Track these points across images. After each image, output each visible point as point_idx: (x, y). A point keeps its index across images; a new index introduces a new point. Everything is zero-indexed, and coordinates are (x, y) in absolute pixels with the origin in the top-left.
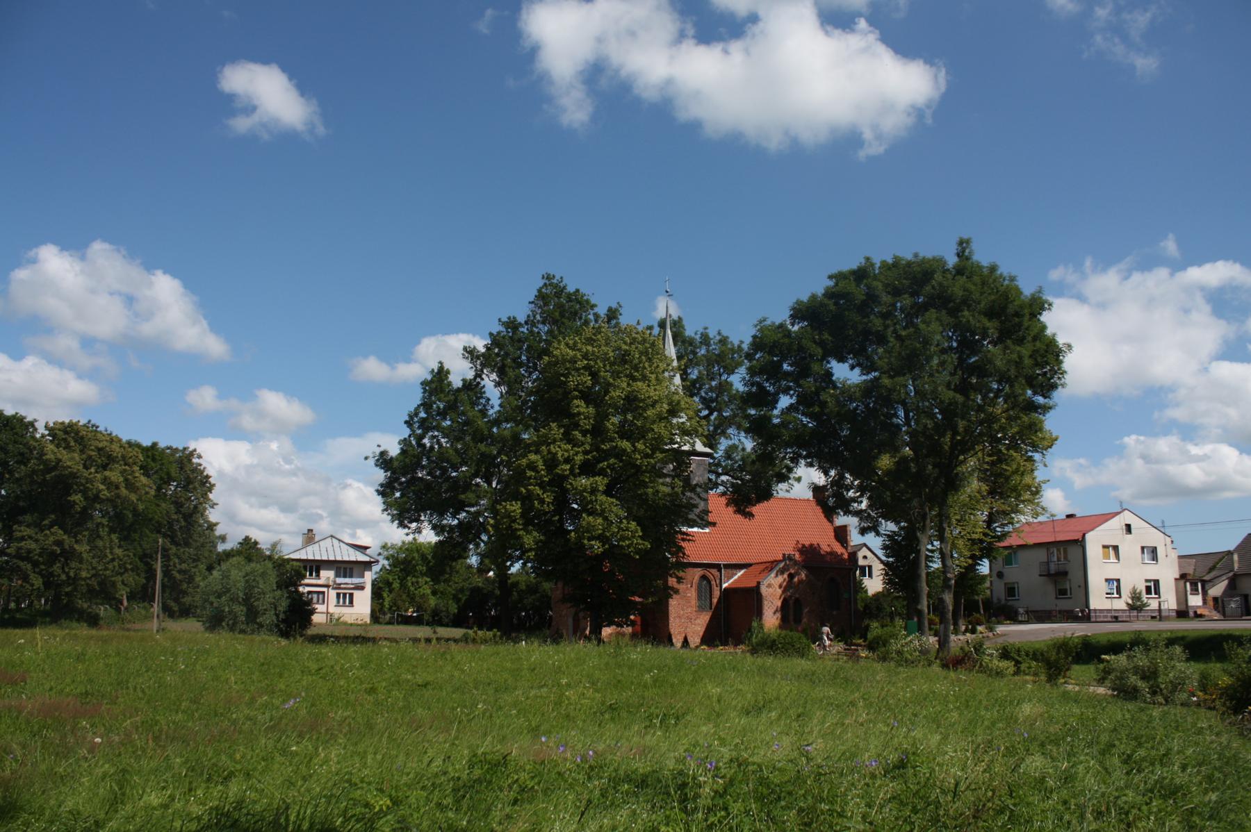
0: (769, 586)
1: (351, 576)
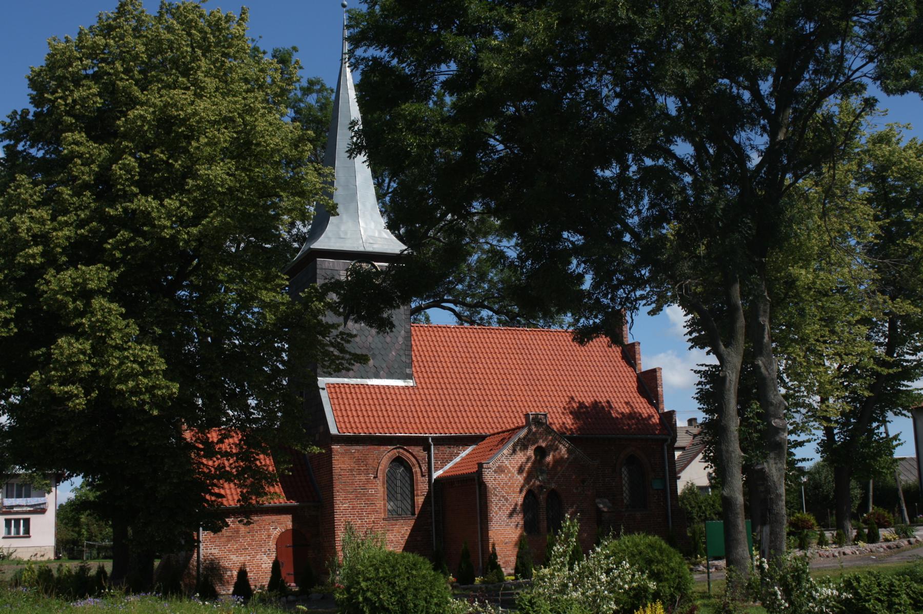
0: (500, 470)
1: (28, 495)
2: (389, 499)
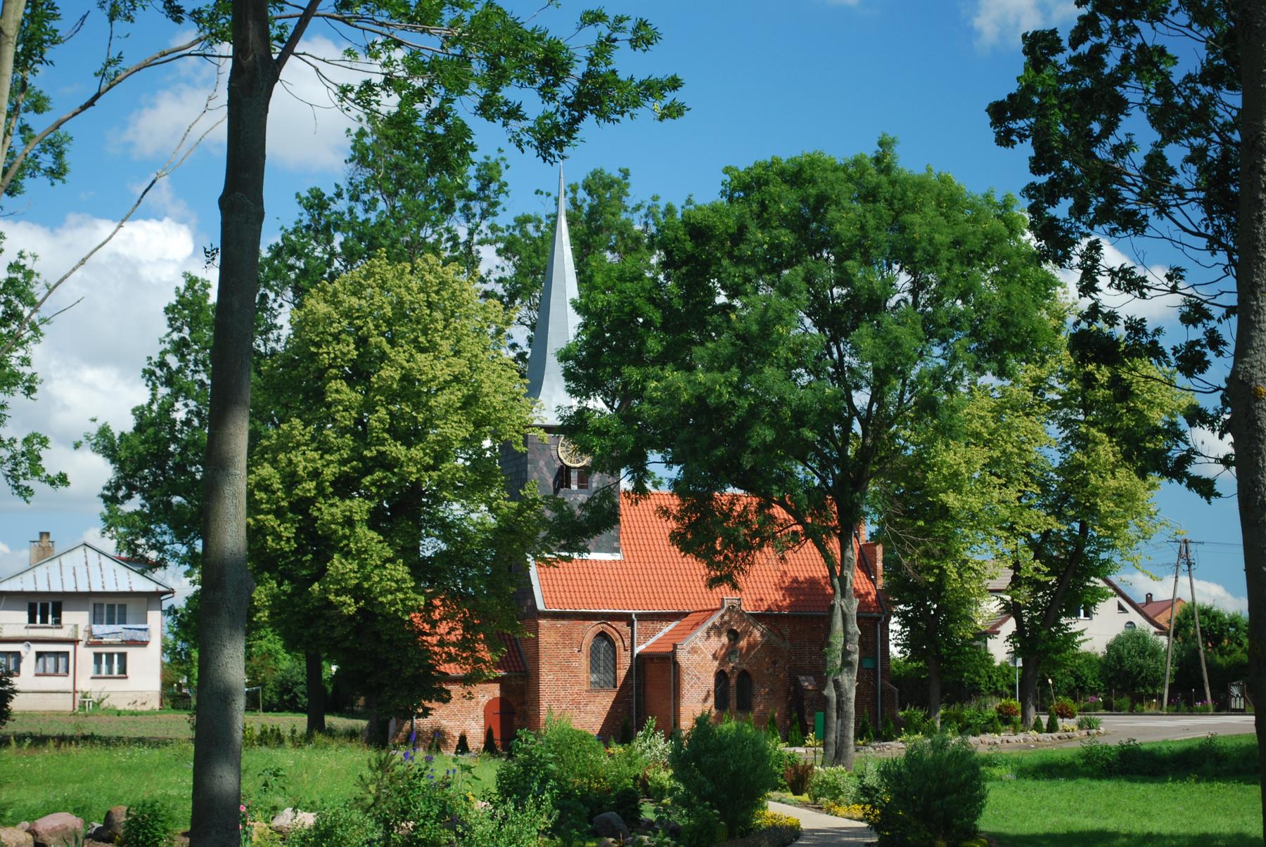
0: (694, 651)
2: (592, 672)
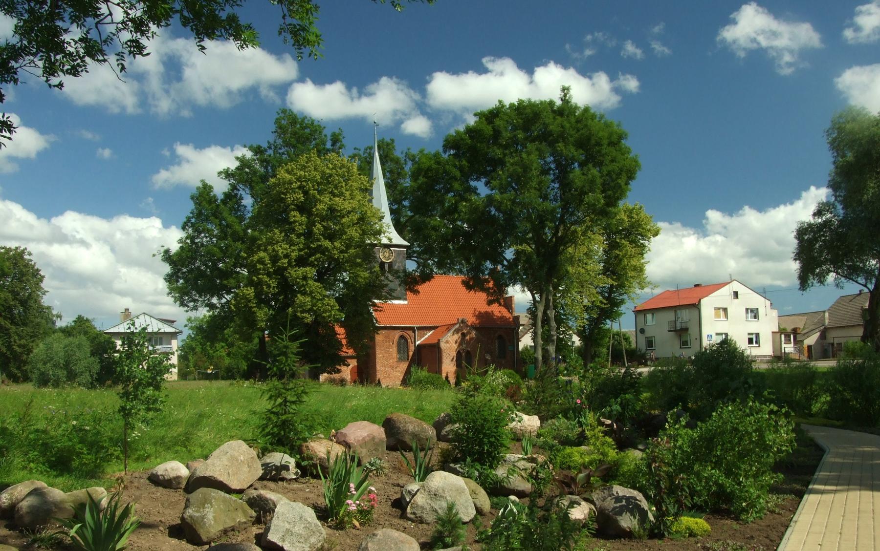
0: (447, 342)
